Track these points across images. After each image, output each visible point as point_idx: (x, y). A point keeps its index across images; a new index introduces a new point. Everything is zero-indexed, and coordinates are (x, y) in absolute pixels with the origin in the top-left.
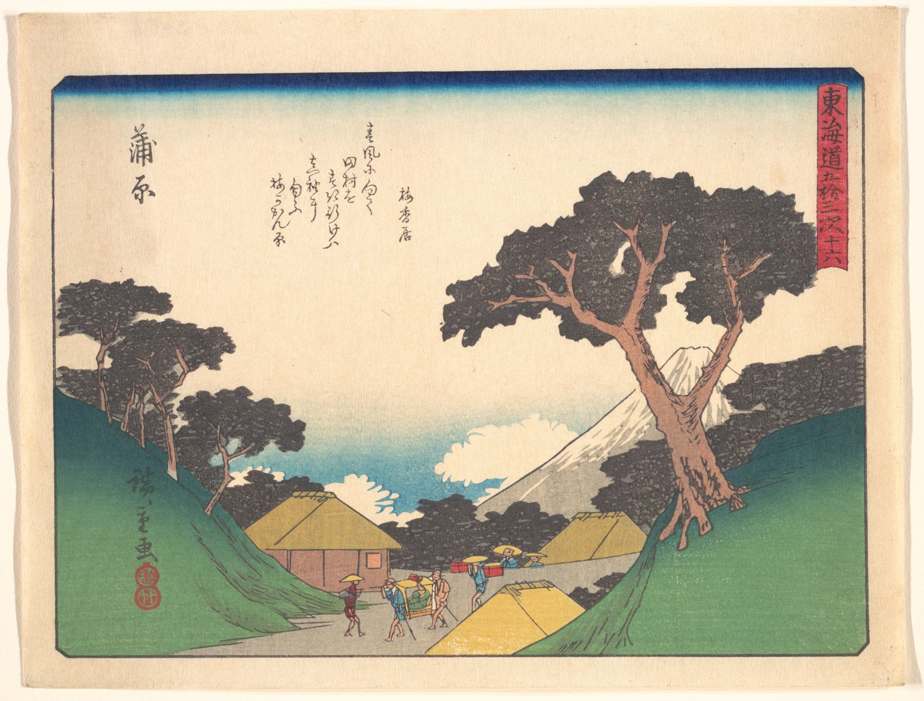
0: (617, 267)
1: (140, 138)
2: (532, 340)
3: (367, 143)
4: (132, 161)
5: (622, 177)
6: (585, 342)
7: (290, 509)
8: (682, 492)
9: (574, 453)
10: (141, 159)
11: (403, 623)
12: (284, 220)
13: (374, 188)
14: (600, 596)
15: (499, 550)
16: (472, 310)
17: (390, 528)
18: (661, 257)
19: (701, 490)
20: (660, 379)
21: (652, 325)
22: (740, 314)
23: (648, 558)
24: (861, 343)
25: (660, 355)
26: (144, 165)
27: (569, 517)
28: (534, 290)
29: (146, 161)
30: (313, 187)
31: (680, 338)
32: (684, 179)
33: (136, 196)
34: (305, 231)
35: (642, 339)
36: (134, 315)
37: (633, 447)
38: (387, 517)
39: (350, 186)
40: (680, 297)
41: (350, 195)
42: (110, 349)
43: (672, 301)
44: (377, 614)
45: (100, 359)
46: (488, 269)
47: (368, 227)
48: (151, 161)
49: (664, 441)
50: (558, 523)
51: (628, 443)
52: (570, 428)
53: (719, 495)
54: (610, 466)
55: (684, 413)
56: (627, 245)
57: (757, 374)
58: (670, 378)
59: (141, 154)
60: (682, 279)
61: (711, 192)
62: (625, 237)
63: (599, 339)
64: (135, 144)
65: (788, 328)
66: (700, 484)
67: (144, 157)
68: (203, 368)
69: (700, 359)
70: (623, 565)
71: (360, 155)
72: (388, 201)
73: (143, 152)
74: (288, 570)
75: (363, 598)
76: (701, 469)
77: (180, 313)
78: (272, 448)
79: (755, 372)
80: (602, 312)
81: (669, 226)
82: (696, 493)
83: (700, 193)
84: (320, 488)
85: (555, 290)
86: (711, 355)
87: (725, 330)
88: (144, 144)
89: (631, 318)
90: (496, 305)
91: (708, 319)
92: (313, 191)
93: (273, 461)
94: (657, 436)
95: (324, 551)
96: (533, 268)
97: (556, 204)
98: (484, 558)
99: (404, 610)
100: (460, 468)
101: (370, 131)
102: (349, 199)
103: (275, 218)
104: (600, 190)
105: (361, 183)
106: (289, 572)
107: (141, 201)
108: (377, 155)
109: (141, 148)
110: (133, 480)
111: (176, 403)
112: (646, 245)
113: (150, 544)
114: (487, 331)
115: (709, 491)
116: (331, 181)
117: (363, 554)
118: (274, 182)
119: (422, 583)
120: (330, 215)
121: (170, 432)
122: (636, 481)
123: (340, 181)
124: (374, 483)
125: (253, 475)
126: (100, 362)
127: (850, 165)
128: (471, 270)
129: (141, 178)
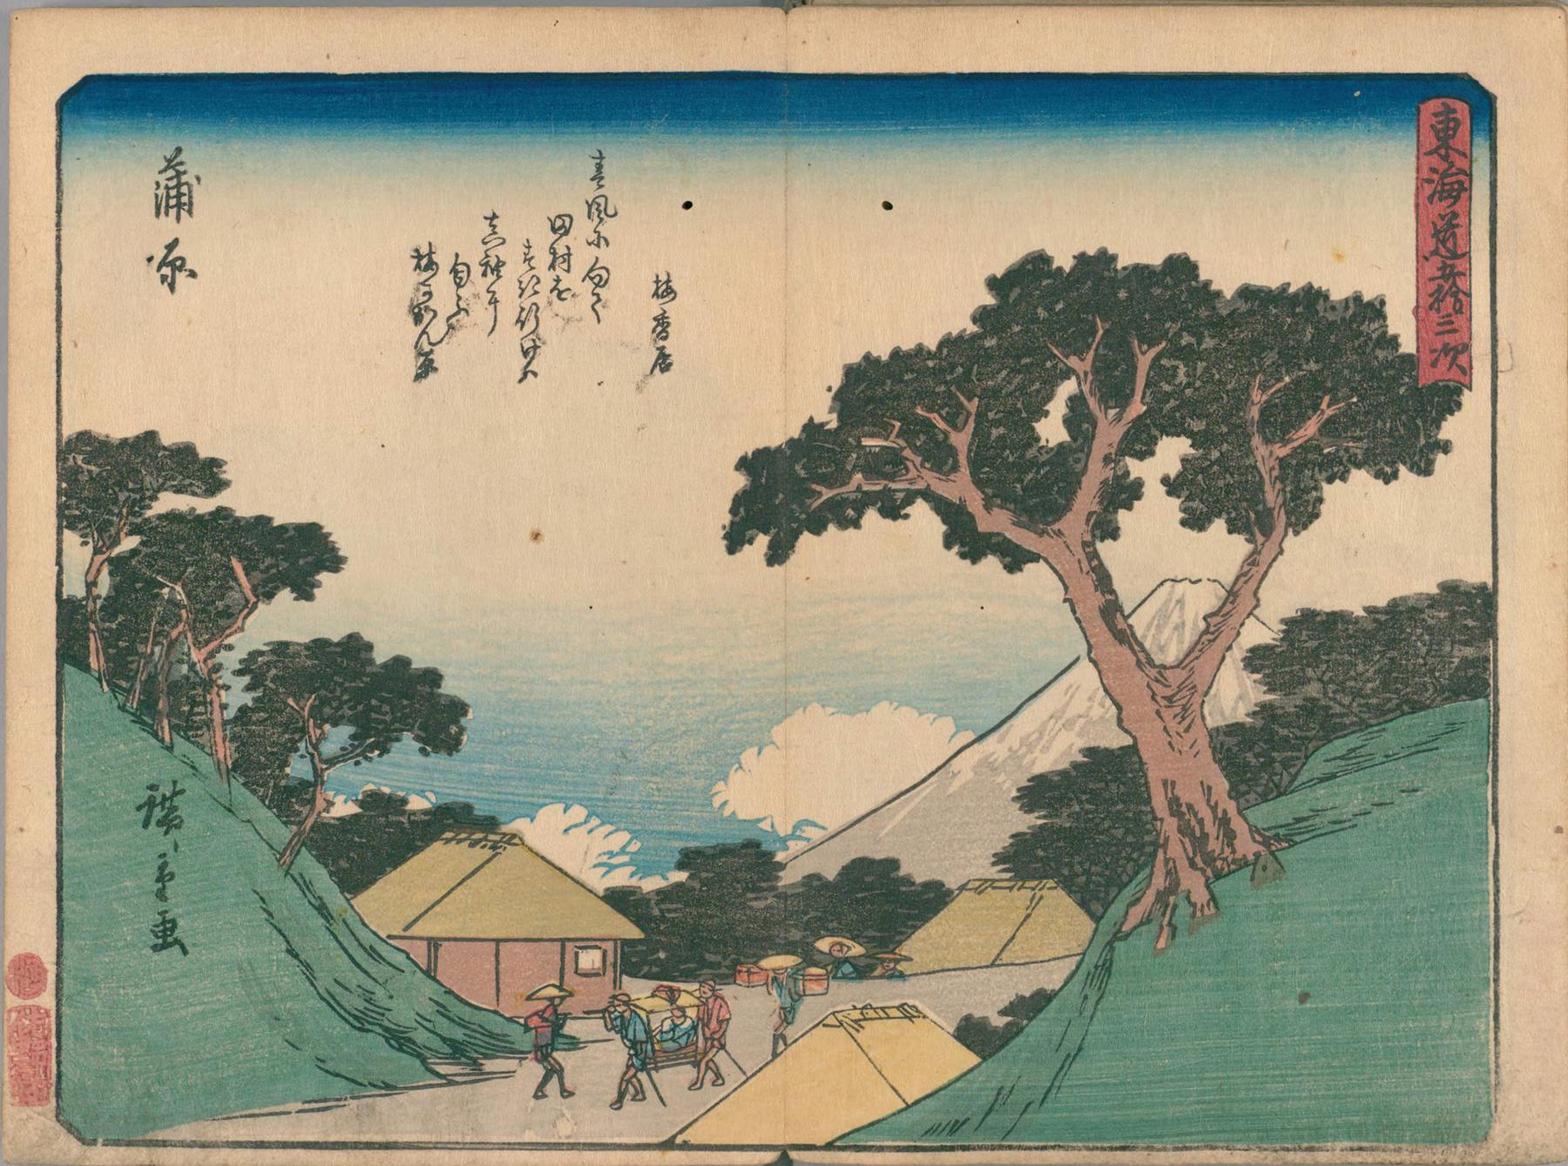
0: (1052, 430)
1: (171, 173)
2: (889, 561)
3: (590, 191)
4: (158, 214)
5: (1064, 261)
7: (443, 859)
8: (1165, 846)
11: (643, 1076)
13: (603, 273)
14: (1012, 1032)
16: (781, 498)
17: (619, 899)
18: (1137, 408)
20: (1125, 637)
23: (1099, 972)
24: (1481, 575)
25: (1127, 589)
26: (178, 219)
27: (952, 883)
28: (889, 464)
29: (184, 214)
30: (494, 268)
31: (1165, 555)
32: (1181, 267)
33: (164, 278)
34: (479, 352)
35: (1095, 563)
36: (154, 498)
37: (1080, 758)
38: (621, 878)
40: (1172, 486)
41: (561, 287)
42: (110, 560)
43: (1154, 491)
46: (811, 428)
48: (190, 212)
49: (1133, 749)
50: (933, 898)
53: (1234, 852)
54: (1037, 792)
55: (1169, 699)
56: (1068, 388)
59: (173, 202)
60: (1172, 452)
62: (1067, 373)
63: (1015, 559)
64: (163, 184)
65: (1369, 543)
66: (1198, 834)
67: (179, 206)
68: (285, 595)
69: (1203, 600)
70: (1052, 977)
71: (579, 213)
74: (430, 974)
75: (571, 1028)
77: (242, 500)
78: (408, 743)
79: (1306, 623)
81: (1152, 353)
82: (1190, 850)
83: (1207, 295)
85: (938, 467)
86: (1223, 593)
87: (1249, 547)
88: (179, 185)
89: (1074, 524)
92: (491, 278)
93: (410, 775)
94: (1115, 740)
96: (898, 424)
99: (646, 1054)
100: (753, 797)
104: (1025, 281)
106: (434, 979)
107: (172, 287)
108: (611, 212)
109: (173, 193)
111: (230, 660)
112: (1115, 391)
113: (173, 921)
115: (1214, 845)
116: (528, 260)
117: (569, 945)
118: (419, 257)
119: (680, 1002)
120: (523, 324)
121: (217, 716)
122: (1084, 828)
123: (542, 259)
126: (91, 585)
128: (778, 431)
129: (171, 247)
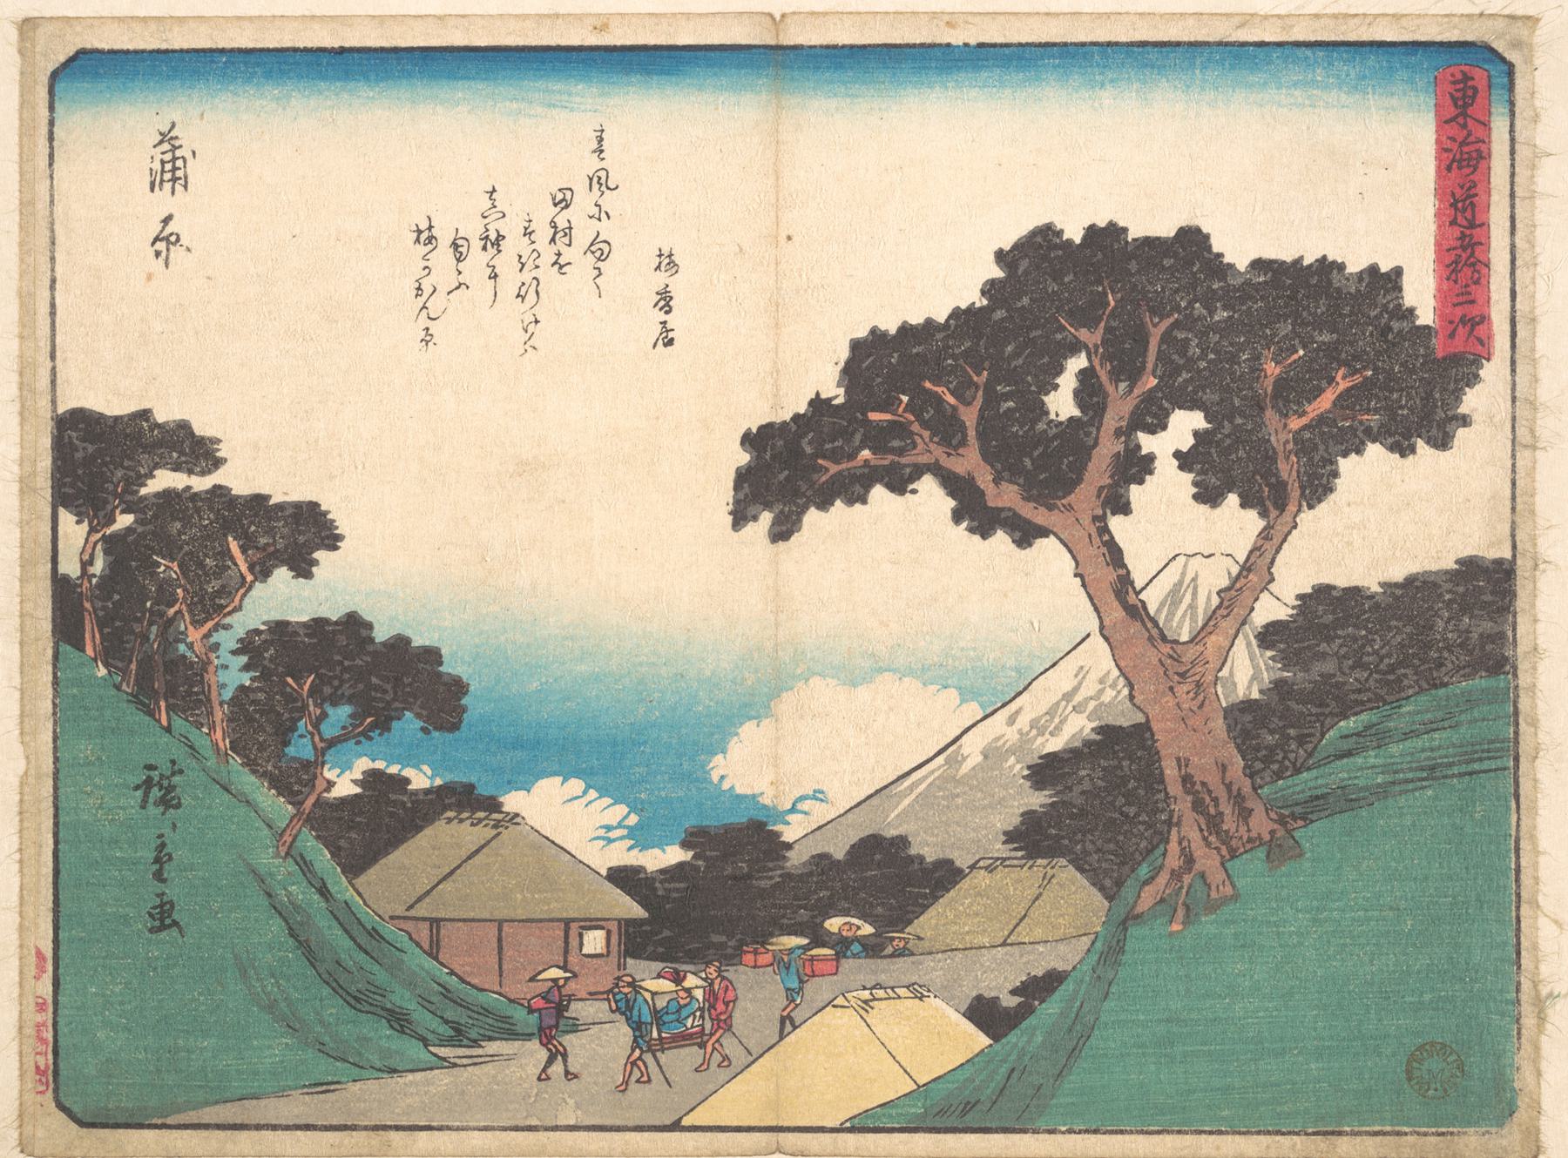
0: (1062, 403)
1: (166, 146)
3: (593, 164)
4: (152, 190)
6: (1001, 540)
8: (1178, 824)
9: (973, 747)
10: (168, 186)
12: (435, 306)
14: (1024, 1011)
15: (834, 924)
16: (787, 473)
17: (623, 877)
19: (1214, 824)
21: (1124, 509)
22: (1295, 493)
23: (1111, 951)
27: (962, 862)
31: (1176, 531)
32: (1192, 240)
33: (158, 254)
38: (621, 855)
39: (561, 241)
40: (1184, 460)
41: (562, 261)
43: (1166, 466)
44: (602, 1043)
45: (86, 557)
46: (818, 403)
47: (597, 314)
48: (186, 187)
51: (1077, 728)
52: (966, 695)
57: (1328, 608)
58: (1159, 610)
59: (168, 176)
60: (1185, 426)
61: (1242, 265)
62: (1074, 348)
63: (1026, 534)
65: (1383, 519)
68: (282, 574)
69: (1214, 577)
71: (580, 187)
72: (632, 276)
73: (171, 172)
75: (576, 1009)
76: (1213, 780)
77: (239, 476)
80: (1033, 480)
84: (493, 805)
87: (1262, 524)
88: (174, 159)
89: (1085, 497)
90: (834, 469)
91: (1233, 499)
92: (492, 251)
94: (1126, 718)
95: (500, 923)
97: (945, 278)
98: (805, 941)
100: (747, 769)
101: (600, 140)
102: (559, 265)
103: (421, 300)
104: (1036, 257)
105: (582, 237)
110: (145, 782)
111: (228, 640)
114: (812, 516)
115: (1229, 824)
117: (574, 926)
119: (687, 984)
122: (1097, 802)
123: (543, 233)
124: (610, 801)
125: (373, 779)
126: (86, 564)
127: (1495, 198)
129: (167, 220)
